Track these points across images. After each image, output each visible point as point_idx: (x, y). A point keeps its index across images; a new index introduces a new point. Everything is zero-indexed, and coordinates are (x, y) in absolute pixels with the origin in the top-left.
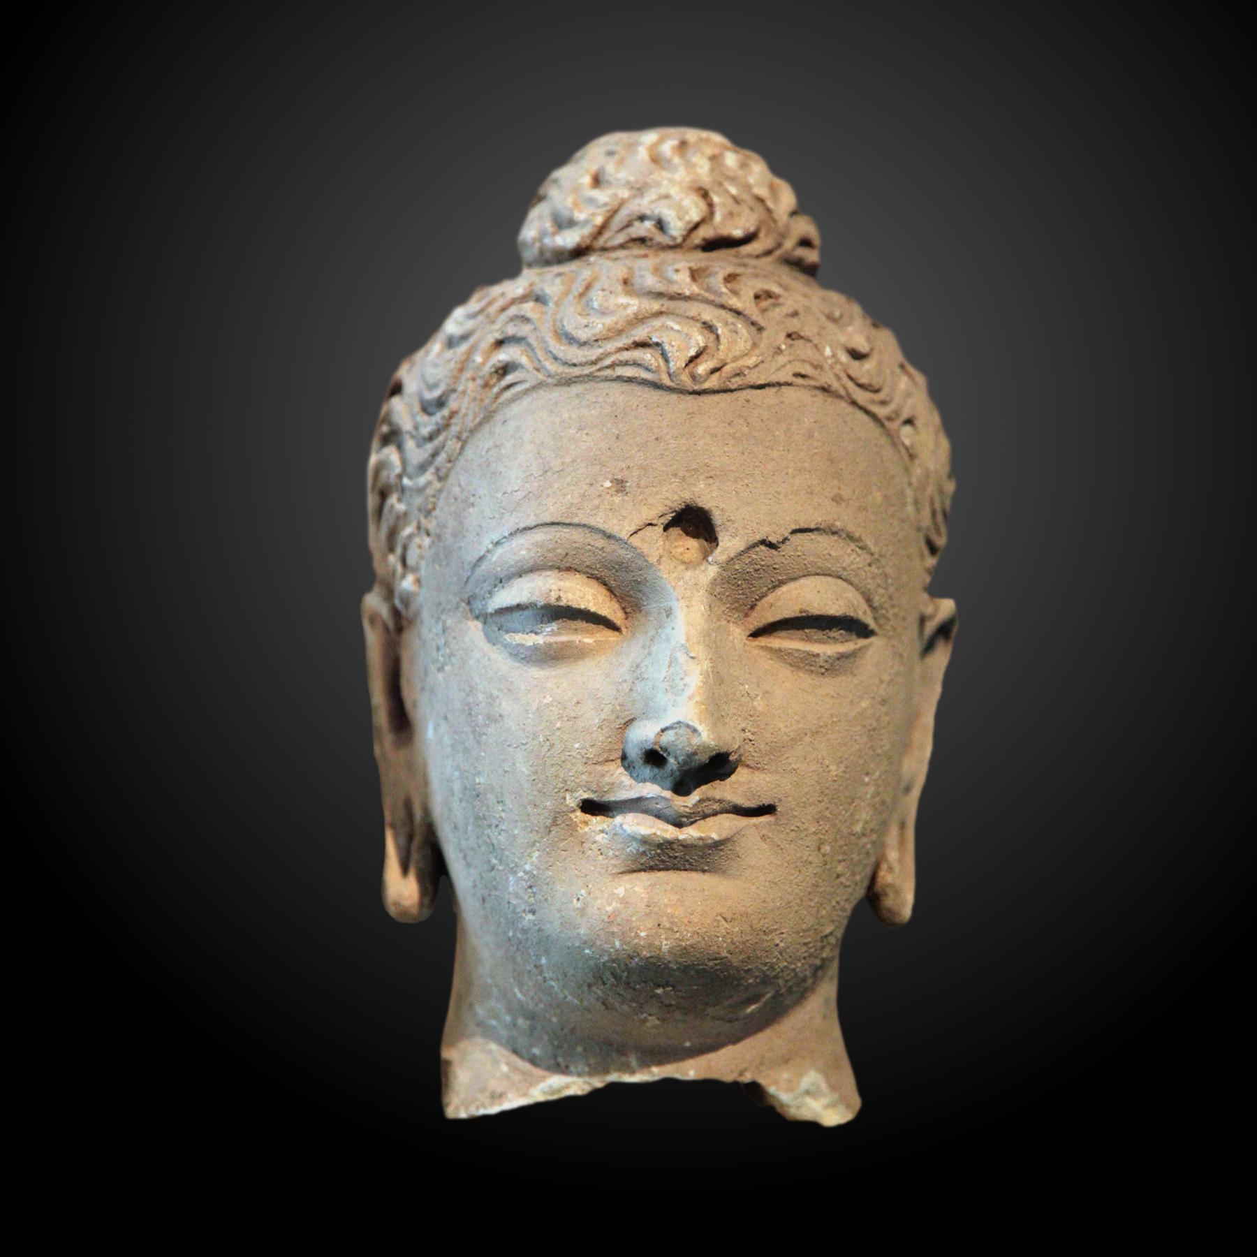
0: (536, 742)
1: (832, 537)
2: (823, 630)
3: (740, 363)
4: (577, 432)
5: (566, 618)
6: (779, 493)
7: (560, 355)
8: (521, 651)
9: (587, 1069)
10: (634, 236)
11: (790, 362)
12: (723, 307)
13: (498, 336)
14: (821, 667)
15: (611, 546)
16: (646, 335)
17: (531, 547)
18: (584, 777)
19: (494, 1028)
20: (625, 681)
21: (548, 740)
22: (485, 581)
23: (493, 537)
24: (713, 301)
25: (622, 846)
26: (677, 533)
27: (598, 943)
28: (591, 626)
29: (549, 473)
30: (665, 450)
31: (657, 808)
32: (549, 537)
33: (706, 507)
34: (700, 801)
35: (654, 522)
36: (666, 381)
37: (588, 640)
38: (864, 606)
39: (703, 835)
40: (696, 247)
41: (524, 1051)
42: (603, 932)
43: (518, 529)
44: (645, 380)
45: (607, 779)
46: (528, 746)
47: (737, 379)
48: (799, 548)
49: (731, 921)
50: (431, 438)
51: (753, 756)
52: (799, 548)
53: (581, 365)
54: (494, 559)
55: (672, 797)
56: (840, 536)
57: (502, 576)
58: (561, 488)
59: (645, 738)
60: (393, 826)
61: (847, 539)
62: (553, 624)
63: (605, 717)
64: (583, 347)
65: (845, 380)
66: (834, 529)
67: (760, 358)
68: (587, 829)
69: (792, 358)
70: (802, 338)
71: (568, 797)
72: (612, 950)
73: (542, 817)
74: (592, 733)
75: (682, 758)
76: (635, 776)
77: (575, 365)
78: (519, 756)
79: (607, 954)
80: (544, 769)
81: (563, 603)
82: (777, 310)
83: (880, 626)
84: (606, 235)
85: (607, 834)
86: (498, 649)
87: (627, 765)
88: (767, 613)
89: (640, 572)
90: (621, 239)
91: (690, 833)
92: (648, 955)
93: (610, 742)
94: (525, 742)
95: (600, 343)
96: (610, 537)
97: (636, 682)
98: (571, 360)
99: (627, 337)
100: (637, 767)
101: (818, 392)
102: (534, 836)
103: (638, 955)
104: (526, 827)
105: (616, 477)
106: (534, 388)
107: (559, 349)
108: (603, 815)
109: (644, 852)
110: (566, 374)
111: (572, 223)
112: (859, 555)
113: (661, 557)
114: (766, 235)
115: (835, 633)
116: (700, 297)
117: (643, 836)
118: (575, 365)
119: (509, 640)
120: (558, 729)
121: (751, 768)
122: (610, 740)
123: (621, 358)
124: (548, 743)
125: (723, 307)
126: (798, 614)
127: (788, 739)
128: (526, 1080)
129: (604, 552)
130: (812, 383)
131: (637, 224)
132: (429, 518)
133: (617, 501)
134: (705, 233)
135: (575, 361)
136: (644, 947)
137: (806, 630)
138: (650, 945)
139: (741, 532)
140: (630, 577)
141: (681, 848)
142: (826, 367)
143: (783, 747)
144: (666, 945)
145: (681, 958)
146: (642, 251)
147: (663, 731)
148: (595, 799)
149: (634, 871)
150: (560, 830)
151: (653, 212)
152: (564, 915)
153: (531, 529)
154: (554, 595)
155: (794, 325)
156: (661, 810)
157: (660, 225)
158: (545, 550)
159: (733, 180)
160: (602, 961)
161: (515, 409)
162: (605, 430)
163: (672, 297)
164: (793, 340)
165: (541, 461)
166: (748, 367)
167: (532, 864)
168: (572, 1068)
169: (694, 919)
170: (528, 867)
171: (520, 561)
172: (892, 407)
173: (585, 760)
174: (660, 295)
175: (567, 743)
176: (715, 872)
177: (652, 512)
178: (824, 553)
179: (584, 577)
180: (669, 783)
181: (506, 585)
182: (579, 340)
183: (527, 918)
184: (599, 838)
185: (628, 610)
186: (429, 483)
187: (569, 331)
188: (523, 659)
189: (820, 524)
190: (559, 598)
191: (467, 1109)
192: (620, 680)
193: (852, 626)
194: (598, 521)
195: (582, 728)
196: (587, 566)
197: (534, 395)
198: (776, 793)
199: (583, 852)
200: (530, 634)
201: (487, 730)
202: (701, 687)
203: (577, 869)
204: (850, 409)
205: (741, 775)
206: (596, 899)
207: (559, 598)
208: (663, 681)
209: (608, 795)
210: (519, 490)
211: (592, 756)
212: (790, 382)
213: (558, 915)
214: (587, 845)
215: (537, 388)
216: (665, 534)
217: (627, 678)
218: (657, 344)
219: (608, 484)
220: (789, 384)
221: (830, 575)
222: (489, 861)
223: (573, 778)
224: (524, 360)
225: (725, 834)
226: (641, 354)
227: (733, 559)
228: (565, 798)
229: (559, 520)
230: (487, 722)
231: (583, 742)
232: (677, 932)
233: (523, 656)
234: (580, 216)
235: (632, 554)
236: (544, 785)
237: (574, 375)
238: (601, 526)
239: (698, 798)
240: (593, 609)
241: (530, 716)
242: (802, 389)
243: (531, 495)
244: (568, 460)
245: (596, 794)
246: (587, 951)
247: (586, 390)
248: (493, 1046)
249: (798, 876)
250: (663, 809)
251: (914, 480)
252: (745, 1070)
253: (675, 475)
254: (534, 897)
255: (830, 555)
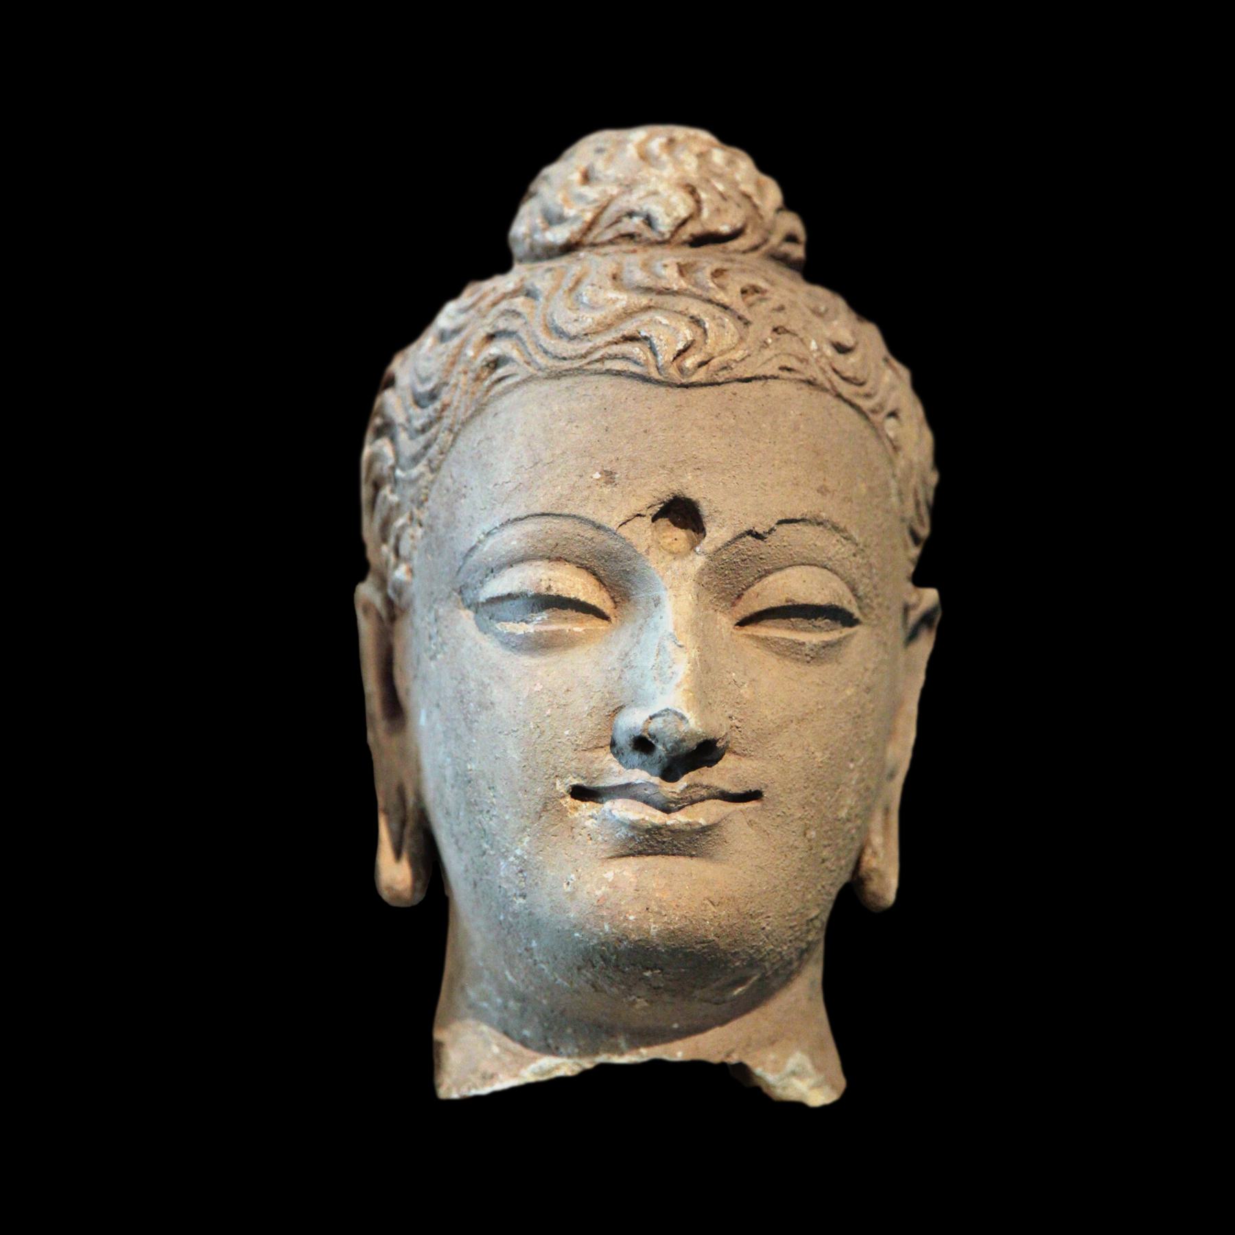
0: (527, 729)
1: (817, 527)
2: (809, 619)
3: (727, 356)
4: (567, 425)
5: (556, 607)
6: (765, 485)
7: (551, 349)
8: (512, 639)
9: (576, 1050)
10: (623, 232)
11: (776, 355)
12: (710, 301)
13: (489, 330)
14: (807, 655)
15: (600, 537)
16: (634, 329)
17: (522, 538)
18: (573, 763)
19: (486, 1010)
20: (614, 669)
21: (538, 727)
22: (476, 571)
23: (485, 528)
24: (701, 296)
25: (611, 831)
26: (665, 523)
27: (588, 926)
28: (581, 615)
29: (539, 465)
30: (654, 442)
31: (645, 794)
32: (539, 527)
33: (694, 498)
34: (688, 787)
35: (642, 513)
36: (655, 374)
37: (578, 629)
38: (849, 595)
39: (690, 820)
40: (684, 243)
41: (514, 1033)
42: (592, 916)
43: (509, 520)
44: (634, 373)
45: (596, 766)
46: (518, 733)
47: (725, 372)
48: (785, 538)
49: (718, 905)
50: (423, 430)
51: (740, 743)
52: (785, 538)
53: (571, 358)
54: (485, 549)
55: (661, 783)
56: (825, 527)
57: (493, 566)
58: (551, 479)
59: (633, 725)
60: (386, 812)
61: (832, 529)
62: (544, 613)
63: (594, 705)
64: (572, 341)
65: (831, 373)
66: (820, 520)
67: (747, 352)
68: (576, 815)
69: (778, 351)
70: (788, 332)
71: (558, 783)
72: (601, 933)
73: (533, 802)
74: (581, 720)
75: (670, 744)
76: (624, 762)
77: (564, 359)
78: (510, 742)
79: (596, 937)
80: (534, 756)
81: (553, 592)
82: (764, 304)
83: (865, 615)
84: (596, 231)
85: (596, 819)
86: (489, 638)
87: (616, 752)
88: (754, 602)
89: (629, 562)
90: (610, 234)
91: (678, 819)
92: (637, 938)
93: (600, 729)
94: (515, 729)
95: (589, 337)
96: (599, 527)
97: (625, 670)
98: (561, 354)
99: (616, 331)
100: (626, 754)
101: (803, 385)
102: (524, 822)
103: (627, 938)
104: (517, 812)
105: (605, 469)
106: (525, 381)
107: (550, 343)
108: (593, 801)
109: (633, 838)
110: (556, 367)
111: (562, 219)
112: (844, 546)
113: (649, 547)
114: (753, 231)
115: (820, 622)
116: (688, 292)
117: (632, 822)
118: (564, 359)
119: (500, 629)
120: (549, 716)
121: (738, 754)
122: (599, 727)
123: (610, 352)
124: (538, 730)
125: (710, 301)
126: (784, 603)
127: (774, 726)
128: (516, 1061)
129: (593, 542)
130: (798, 376)
131: (626, 220)
132: (422, 509)
133: (606, 493)
134: (693, 228)
135: (565, 355)
136: (633, 930)
137: (792, 619)
138: (639, 928)
139: (728, 522)
140: (619, 567)
141: (669, 833)
142: (812, 360)
143: (770, 734)
144: (655, 928)
145: (669, 941)
146: (631, 247)
147: (651, 718)
148: (585, 785)
149: (623, 856)
150: (550, 815)
151: (641, 209)
152: (554, 899)
153: (521, 519)
154: (544, 585)
155: (780, 319)
156: (649, 796)
157: (649, 221)
158: (535, 540)
159: (720, 176)
160: (592, 944)
161: (506, 401)
162: (594, 422)
163: (660, 292)
164: (779, 334)
165: (531, 453)
166: (735, 361)
167: (522, 849)
168: (562, 1050)
169: (682, 903)
170: (518, 852)
171: (511, 551)
172: (876, 400)
173: (574, 747)
174: (648, 290)
175: (557, 730)
176: (703, 856)
177: (640, 504)
178: (810, 543)
179: (574, 567)
180: (657, 769)
181: (497, 575)
182: (569, 334)
183: (518, 902)
184: (589, 823)
185: (617, 600)
186: (422, 475)
187: (560, 325)
188: (513, 647)
189: (806, 515)
190: (549, 588)
191: (458, 1090)
192: (609, 668)
193: (837, 615)
194: (587, 512)
195: (572, 715)
196: (577, 557)
197: (525, 388)
198: (763, 779)
199: (573, 837)
200: (520, 623)
201: (479, 718)
202: (688, 675)
203: (566, 854)
204: (835, 402)
205: (728, 762)
206: (585, 883)
207: (549, 588)
208: (652, 669)
209: (597, 782)
210: (510, 481)
211: (581, 743)
212: (776, 375)
213: (548, 899)
214: (576, 830)
215: (528, 381)
216: (654, 524)
217: (616, 666)
218: (646, 338)
219: (597, 476)
220: (775, 377)
221: (815, 565)
222: (481, 846)
223: (563, 765)
224: (515, 354)
225: (712, 820)
226: (630, 348)
227: (720, 549)
228: (555, 784)
229: (550, 511)
230: (479, 710)
231: (572, 729)
232: (665, 915)
233: (514, 645)
234: (570, 212)
235: (621, 544)
236: (534, 771)
237: (564, 368)
238: (591, 517)
239: (685, 784)
240: (582, 599)
241: (521, 703)
242: (788, 382)
243: (522, 486)
244: (558, 452)
245: (586, 781)
246: (577, 935)
247: (576, 383)
248: (485, 1028)
249: (784, 860)
250: (652, 794)
251: (898, 472)
252: (732, 1051)
253: (663, 467)
254: (524, 881)
255: (816, 545)
